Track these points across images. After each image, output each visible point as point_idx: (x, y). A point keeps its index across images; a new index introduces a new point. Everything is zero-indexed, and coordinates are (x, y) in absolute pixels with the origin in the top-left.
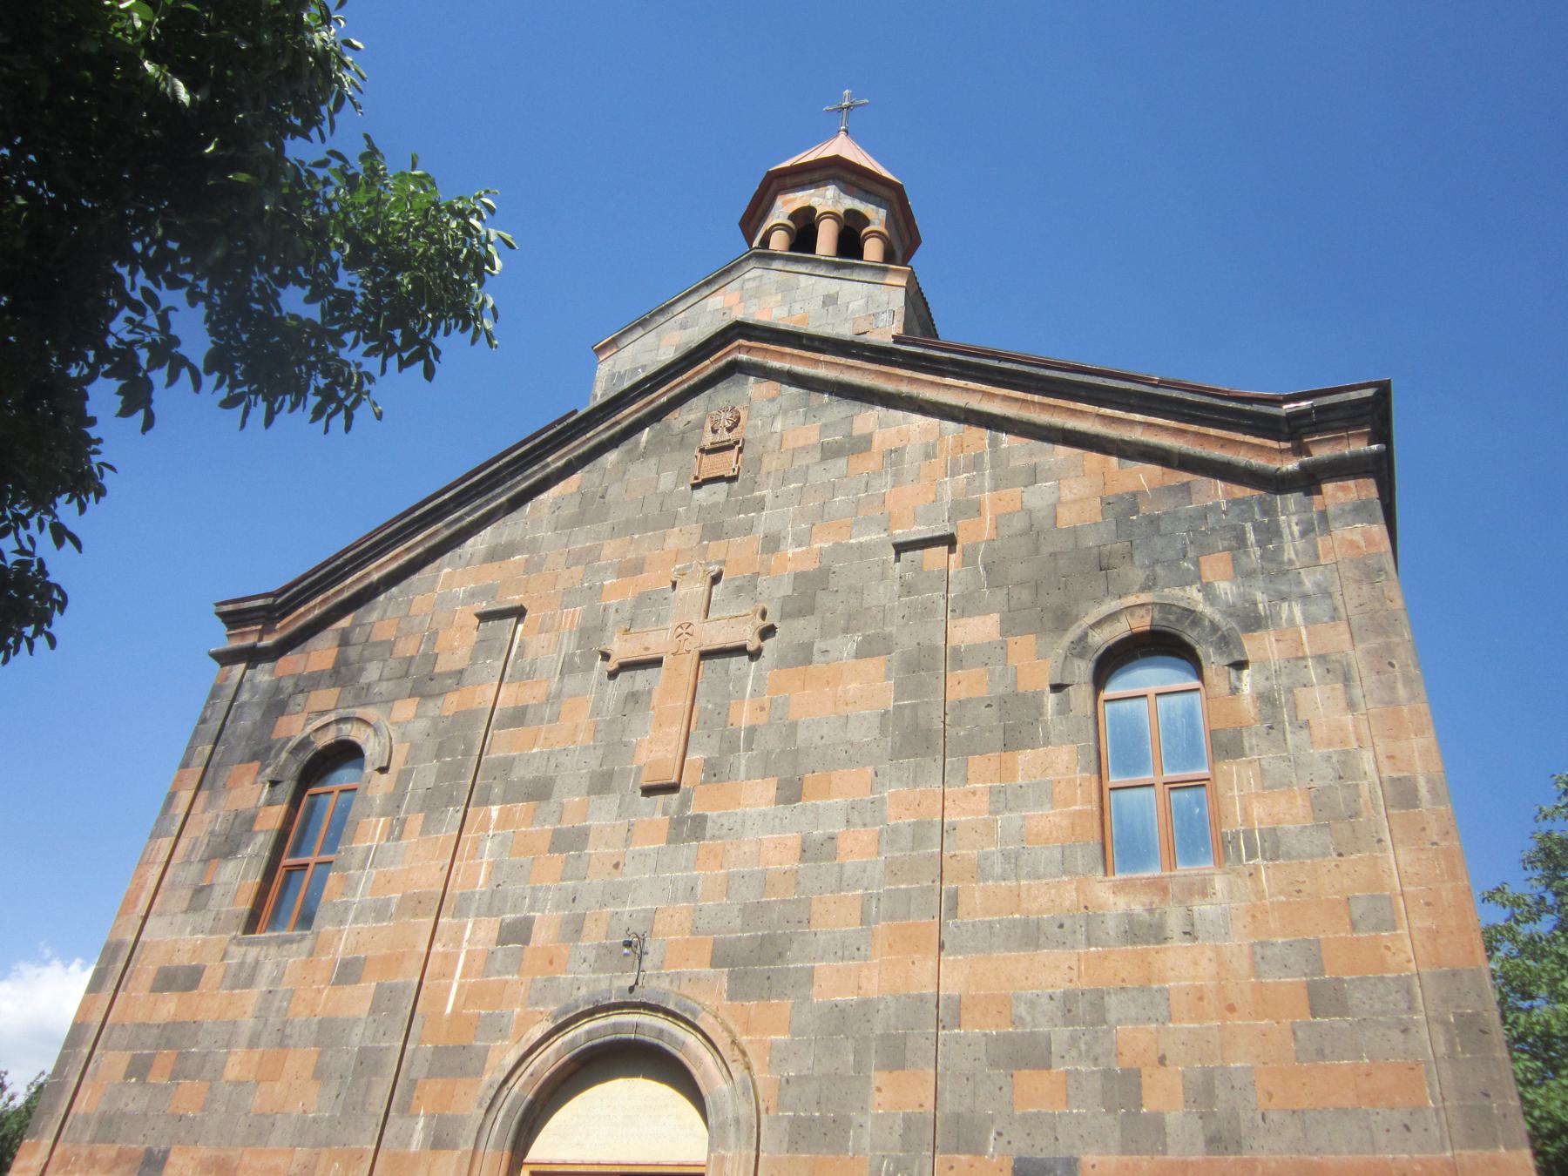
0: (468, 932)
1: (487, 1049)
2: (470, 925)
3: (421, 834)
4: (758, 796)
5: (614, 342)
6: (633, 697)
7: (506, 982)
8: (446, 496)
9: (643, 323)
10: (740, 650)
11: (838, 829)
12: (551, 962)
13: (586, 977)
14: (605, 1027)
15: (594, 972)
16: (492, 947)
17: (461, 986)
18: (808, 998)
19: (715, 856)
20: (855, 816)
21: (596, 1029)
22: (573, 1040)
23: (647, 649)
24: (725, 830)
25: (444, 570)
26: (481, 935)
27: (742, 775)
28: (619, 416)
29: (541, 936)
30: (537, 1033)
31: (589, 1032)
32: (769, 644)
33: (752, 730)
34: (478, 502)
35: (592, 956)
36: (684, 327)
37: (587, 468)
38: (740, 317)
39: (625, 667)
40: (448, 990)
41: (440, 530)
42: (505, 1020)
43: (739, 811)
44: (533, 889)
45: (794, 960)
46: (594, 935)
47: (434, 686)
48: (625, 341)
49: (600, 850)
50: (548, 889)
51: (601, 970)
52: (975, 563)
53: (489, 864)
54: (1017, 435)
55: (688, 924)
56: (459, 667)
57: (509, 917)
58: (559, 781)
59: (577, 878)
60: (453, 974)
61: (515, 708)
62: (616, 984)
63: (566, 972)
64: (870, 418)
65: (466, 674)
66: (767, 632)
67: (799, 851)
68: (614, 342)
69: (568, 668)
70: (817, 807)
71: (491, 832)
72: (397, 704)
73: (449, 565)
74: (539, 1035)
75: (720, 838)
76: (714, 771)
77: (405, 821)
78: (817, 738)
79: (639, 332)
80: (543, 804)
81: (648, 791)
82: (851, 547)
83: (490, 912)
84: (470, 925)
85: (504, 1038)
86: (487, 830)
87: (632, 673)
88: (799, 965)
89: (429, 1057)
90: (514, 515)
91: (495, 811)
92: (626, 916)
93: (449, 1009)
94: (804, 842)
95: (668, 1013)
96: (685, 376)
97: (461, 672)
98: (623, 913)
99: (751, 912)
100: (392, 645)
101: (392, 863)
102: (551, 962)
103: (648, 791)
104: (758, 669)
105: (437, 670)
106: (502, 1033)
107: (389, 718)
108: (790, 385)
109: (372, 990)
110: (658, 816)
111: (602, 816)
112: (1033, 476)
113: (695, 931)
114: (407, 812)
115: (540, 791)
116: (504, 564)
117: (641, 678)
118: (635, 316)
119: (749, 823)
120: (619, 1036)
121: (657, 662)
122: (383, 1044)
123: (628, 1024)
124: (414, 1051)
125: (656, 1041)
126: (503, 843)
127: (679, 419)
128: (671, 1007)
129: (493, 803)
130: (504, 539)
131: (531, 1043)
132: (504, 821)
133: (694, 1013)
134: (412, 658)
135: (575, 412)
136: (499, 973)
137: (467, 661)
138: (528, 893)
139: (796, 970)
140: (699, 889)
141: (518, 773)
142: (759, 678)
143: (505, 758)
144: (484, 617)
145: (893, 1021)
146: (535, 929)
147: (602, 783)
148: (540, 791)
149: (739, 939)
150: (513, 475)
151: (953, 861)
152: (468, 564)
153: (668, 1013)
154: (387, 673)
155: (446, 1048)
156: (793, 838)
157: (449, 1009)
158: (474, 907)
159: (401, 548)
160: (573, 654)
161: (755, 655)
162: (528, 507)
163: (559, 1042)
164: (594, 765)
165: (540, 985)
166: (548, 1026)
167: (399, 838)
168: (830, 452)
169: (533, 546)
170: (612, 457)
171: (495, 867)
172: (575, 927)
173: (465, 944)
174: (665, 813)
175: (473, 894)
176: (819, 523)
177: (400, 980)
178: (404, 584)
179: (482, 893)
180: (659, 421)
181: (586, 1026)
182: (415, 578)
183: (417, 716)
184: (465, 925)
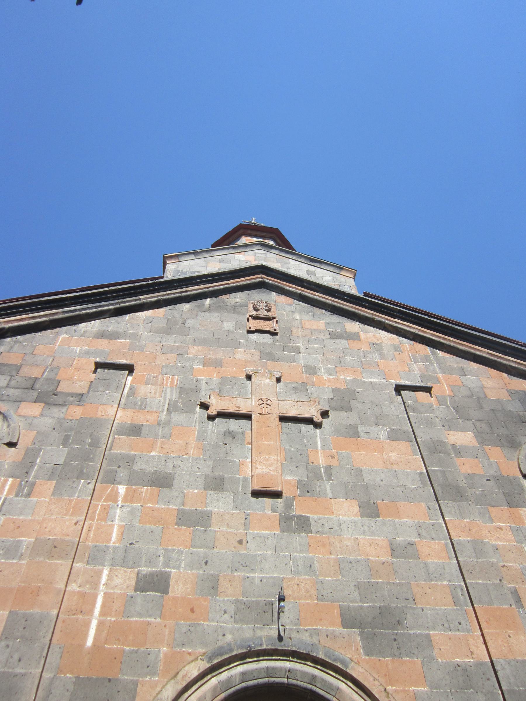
0: (104, 579)
1: (136, 684)
2: (106, 572)
3: (53, 494)
4: (346, 511)
5: (177, 256)
6: (230, 434)
7: (149, 624)
8: (69, 295)
9: (195, 253)
10: (309, 421)
11: (414, 539)
12: (192, 611)
13: (230, 626)
14: (258, 670)
15: (236, 622)
16: (133, 593)
17: (100, 624)
18: (433, 659)
19: (324, 545)
20: (423, 532)
21: (251, 672)
22: (229, 679)
23: (238, 407)
24: (326, 529)
25: (63, 334)
26: (118, 581)
27: (330, 495)
28: (188, 289)
29: (178, 588)
30: (193, 670)
31: (243, 674)
32: (325, 421)
33: (329, 469)
34: (89, 306)
35: (232, 609)
36: (221, 261)
37: (169, 307)
38: (264, 263)
39: (221, 415)
40: (87, 625)
41: (42, 316)
42: (152, 657)
43: (334, 517)
44: (166, 550)
45: (412, 628)
46: (229, 593)
47: (59, 399)
48: (183, 258)
49: (224, 529)
50: (180, 552)
51: (242, 621)
52: (446, 405)
53: (120, 527)
54: (445, 352)
55: (314, 592)
56: (80, 391)
57: (145, 570)
58: (177, 476)
59: (208, 547)
60: (91, 612)
61: (131, 424)
62: (265, 635)
63: (208, 620)
64: (354, 326)
65: (84, 397)
66: (325, 414)
67: (389, 549)
68: (177, 256)
69: (172, 408)
70: (394, 522)
71: (120, 503)
72: (23, 404)
73: (66, 333)
74: (195, 673)
75: (323, 533)
76: (306, 489)
77: (33, 485)
78: (378, 480)
79: (192, 257)
80: (166, 490)
81: (257, 494)
82: (365, 382)
83: (124, 563)
84: (106, 572)
85: (153, 674)
86: (116, 501)
87: (227, 420)
88: (418, 632)
89: (71, 688)
90: (116, 318)
91: (122, 489)
92: (257, 581)
93: (89, 642)
94: (391, 544)
95: (317, 661)
96: (229, 282)
97: (82, 395)
98: (253, 578)
99: (365, 589)
100: (18, 369)
101: (21, 513)
102: (192, 611)
103: (257, 494)
104: (322, 434)
105: (59, 389)
106: (150, 669)
107: (16, 412)
108: (299, 301)
109: (6, 616)
110: (269, 512)
111: (220, 505)
112: (463, 373)
113: (321, 598)
114: (36, 477)
115: (162, 481)
116: (112, 342)
117: (234, 424)
118: (191, 250)
119: (344, 527)
120: (272, 680)
121: (248, 417)
122: (18, 670)
123: (281, 669)
124: (52, 680)
125: (310, 686)
126: (132, 512)
127: (231, 299)
128: (321, 656)
129: (120, 483)
130: (110, 328)
131: (188, 680)
132: (129, 498)
133: (343, 662)
134: (36, 379)
135: (162, 278)
136: (140, 615)
137: (86, 389)
138: (161, 552)
139: (417, 635)
140: (317, 567)
141: (139, 466)
142: (323, 440)
143: (127, 455)
144: (99, 366)
145: (512, 680)
146: (172, 582)
147: (216, 484)
148: (162, 481)
149: (361, 607)
150: (115, 298)
151: (505, 569)
152: (82, 336)
153: (317, 661)
154: (13, 383)
155: (89, 679)
156: (381, 540)
157: (89, 642)
158: (108, 557)
159: (27, 316)
160: (176, 401)
161: (318, 426)
162: (127, 317)
163: (213, 681)
164: (207, 471)
165: (184, 629)
166: (204, 665)
167: (29, 495)
168: (333, 336)
169: (134, 337)
170: (186, 306)
171: (124, 531)
172: (212, 585)
173: (102, 587)
174: (274, 511)
175: (108, 548)
176: (339, 366)
177: (36, 611)
178: (27, 336)
179: (115, 548)
180: (216, 297)
181: (238, 669)
182: (38, 335)
183: (42, 415)
184: (101, 572)
